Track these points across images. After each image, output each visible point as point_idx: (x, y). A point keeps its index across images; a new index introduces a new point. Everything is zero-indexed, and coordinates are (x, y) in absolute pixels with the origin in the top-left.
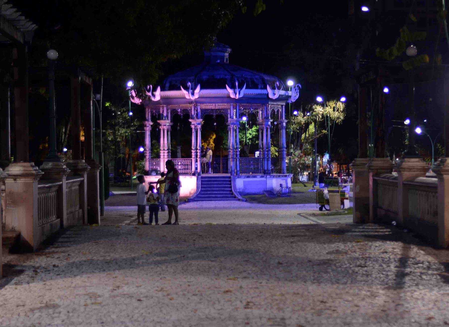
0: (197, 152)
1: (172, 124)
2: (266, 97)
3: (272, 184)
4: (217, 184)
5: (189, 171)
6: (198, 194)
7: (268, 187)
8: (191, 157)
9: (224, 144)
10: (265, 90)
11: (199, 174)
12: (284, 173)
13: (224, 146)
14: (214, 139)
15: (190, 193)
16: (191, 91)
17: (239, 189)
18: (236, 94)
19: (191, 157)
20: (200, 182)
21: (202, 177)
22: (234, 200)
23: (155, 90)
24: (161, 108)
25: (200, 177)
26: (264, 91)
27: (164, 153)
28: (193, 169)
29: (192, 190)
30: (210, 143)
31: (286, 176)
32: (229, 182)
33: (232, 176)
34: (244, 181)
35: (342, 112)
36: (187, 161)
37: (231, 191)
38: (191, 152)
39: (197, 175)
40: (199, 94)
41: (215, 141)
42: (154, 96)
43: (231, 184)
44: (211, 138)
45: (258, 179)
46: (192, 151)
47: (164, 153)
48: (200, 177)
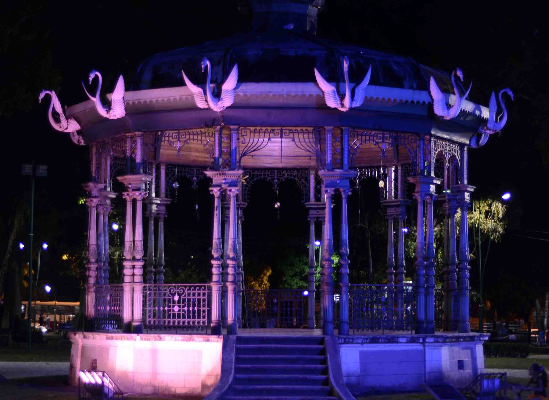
0: (224, 267)
1: (168, 201)
2: (425, 112)
3: (440, 361)
5: (202, 320)
6: (226, 393)
7: (428, 370)
8: (209, 277)
9: (285, 282)
10: (424, 93)
11: (231, 330)
12: (466, 331)
13: (284, 286)
14: (270, 276)
15: (204, 386)
16: (210, 86)
17: (348, 376)
18: (342, 97)
21: (240, 340)
23: (110, 88)
24: (128, 146)
25: (233, 337)
26: (420, 96)
27: (134, 267)
29: (209, 375)
30: (262, 281)
31: (472, 338)
32: (320, 354)
33: (327, 338)
34: (362, 353)
35: (500, 220)
37: (326, 382)
38: (211, 266)
39: (224, 332)
40: (236, 96)
41: (270, 278)
42: (107, 104)
43: (324, 361)
44: (265, 274)
45: (402, 347)
46: (214, 262)
47: (134, 267)
48: (233, 337)
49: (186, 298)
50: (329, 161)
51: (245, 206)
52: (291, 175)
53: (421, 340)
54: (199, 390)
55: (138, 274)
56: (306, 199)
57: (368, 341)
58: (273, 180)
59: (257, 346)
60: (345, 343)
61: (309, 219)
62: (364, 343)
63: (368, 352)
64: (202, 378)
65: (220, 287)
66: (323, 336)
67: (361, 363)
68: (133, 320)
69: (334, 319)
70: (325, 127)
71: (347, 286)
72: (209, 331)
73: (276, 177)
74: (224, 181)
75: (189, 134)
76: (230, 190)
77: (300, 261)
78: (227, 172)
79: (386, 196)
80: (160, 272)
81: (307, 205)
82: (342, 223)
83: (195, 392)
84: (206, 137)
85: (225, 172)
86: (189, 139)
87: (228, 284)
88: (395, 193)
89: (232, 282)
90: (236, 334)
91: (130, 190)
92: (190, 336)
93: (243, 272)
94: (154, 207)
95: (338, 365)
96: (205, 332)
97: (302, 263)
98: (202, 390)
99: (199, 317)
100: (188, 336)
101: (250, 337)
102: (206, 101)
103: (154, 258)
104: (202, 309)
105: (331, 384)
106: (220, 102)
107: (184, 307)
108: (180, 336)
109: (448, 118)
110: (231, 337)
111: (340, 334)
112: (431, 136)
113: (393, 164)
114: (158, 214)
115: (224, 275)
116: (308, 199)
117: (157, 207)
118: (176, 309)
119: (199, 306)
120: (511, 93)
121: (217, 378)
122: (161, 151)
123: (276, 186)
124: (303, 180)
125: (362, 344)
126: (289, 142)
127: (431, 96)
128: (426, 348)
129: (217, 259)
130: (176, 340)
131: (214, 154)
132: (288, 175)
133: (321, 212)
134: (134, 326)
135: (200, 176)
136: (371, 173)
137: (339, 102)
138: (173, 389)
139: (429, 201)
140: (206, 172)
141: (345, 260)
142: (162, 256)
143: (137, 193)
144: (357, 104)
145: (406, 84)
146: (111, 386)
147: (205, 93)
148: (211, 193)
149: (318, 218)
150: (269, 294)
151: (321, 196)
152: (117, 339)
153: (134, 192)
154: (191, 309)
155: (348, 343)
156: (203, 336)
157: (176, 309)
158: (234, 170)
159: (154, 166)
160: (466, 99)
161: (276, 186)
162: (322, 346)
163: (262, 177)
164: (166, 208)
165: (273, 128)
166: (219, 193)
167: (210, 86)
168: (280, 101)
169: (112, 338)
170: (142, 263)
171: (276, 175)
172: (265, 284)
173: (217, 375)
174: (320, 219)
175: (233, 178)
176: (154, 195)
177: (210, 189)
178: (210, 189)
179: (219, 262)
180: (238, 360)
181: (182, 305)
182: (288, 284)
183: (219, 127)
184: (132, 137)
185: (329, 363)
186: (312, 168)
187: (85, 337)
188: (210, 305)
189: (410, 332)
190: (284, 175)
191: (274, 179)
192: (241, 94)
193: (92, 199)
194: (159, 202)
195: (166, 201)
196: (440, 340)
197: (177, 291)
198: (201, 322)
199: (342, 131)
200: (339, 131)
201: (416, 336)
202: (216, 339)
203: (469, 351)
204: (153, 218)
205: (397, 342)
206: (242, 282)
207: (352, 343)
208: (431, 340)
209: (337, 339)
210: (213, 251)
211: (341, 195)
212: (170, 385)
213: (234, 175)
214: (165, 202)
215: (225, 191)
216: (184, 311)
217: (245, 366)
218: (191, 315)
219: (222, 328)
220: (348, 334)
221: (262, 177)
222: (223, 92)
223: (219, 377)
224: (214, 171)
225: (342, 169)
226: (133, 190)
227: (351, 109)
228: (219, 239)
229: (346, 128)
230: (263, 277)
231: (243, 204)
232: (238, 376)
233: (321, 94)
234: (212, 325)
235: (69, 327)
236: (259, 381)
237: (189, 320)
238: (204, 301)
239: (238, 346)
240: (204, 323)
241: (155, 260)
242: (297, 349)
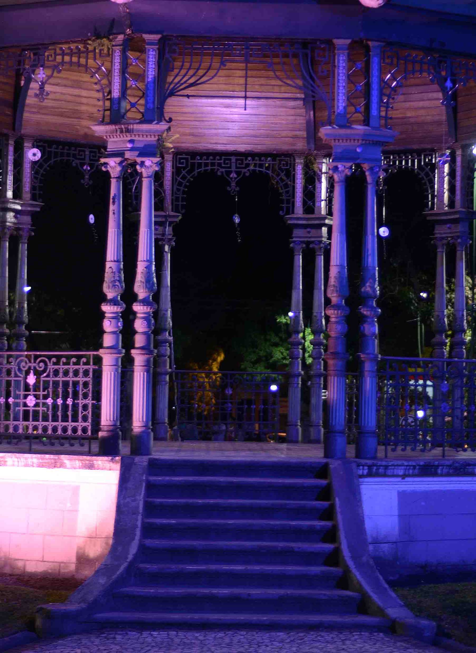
0: (128, 317)
1: (37, 206)
4: (244, 511)
5: (80, 424)
6: (122, 580)
11: (139, 446)
14: (222, 362)
15: (82, 559)
17: (376, 542)
19: (99, 346)
20: (141, 498)
21: (156, 466)
22: (359, 627)
25: (142, 461)
28: (108, 413)
32: (320, 497)
33: (334, 464)
34: (402, 495)
36: (69, 368)
37: (334, 558)
38: (102, 315)
39: (125, 448)
41: (222, 366)
43: (329, 514)
44: (215, 360)
46: (105, 308)
48: (142, 461)
49: (51, 379)
50: (341, 108)
51: (177, 220)
52: (261, 166)
54: (72, 567)
56: (288, 209)
57: (416, 471)
58: (229, 173)
59: (191, 478)
60: (370, 475)
61: (291, 245)
62: (409, 476)
63: (414, 493)
64: (80, 542)
65: (117, 359)
66: (325, 460)
67: (401, 516)
70: (335, 41)
72: (95, 447)
73: (233, 169)
74: (129, 145)
75: (63, 54)
76: (142, 164)
77: (266, 340)
78: (136, 127)
79: (433, 204)
80: (18, 337)
81: (291, 219)
82: (366, 234)
83: (62, 571)
84: (95, 59)
85: (131, 127)
86: (63, 63)
87: (133, 351)
88: (450, 198)
89: (141, 348)
90: (148, 454)
92: (56, 457)
93: (171, 338)
94: (10, 216)
95: (357, 521)
96: (86, 449)
97: (268, 343)
98: (77, 569)
99: (75, 419)
100: (52, 456)
101: (178, 461)
103: (7, 310)
104: (81, 402)
105: (345, 562)
107: (46, 397)
108: (34, 456)
110: (137, 459)
111: (359, 455)
113: (448, 145)
114: (18, 229)
115: (127, 333)
116: (291, 210)
117: (15, 217)
118: (31, 401)
119: (75, 396)
121: (107, 543)
122: (26, 115)
123: (233, 184)
124: (283, 175)
125: (404, 476)
126: (258, 107)
129: (114, 302)
130: (26, 465)
131: (110, 92)
133: (314, 232)
136: (407, 163)
138: (20, 564)
141: (372, 307)
142: (23, 307)
148: (104, 169)
149: (308, 243)
150: (219, 391)
151: (314, 205)
154: (70, 401)
155: (377, 475)
156: (81, 457)
157: (31, 401)
159: (11, 142)
161: (233, 184)
162: (324, 482)
163: (209, 168)
164: (32, 220)
166: (119, 169)
171: (233, 165)
173: (107, 538)
174: (311, 246)
175: (149, 139)
176: (10, 194)
177: (103, 160)
178: (103, 160)
180: (150, 509)
182: (248, 374)
183: (121, 37)
185: (339, 517)
186: (301, 153)
188: (97, 396)
190: (248, 165)
191: (231, 172)
194: (19, 207)
195: (32, 205)
197: (33, 365)
198: (40, 427)
202: (108, 465)
204: (8, 236)
206: (170, 357)
207: (385, 475)
209: (354, 466)
210: (105, 285)
211: (365, 176)
212: (14, 555)
213: (149, 133)
214: (29, 209)
215: (134, 164)
217: (165, 521)
218: (59, 414)
219: (120, 442)
220: (375, 458)
221: (209, 168)
223: (111, 542)
225: (368, 125)
228: (118, 261)
229: (376, 44)
230: (212, 365)
231: (174, 216)
232: (148, 542)
236: (192, 555)
239: (152, 478)
240: (84, 430)
241: (11, 314)
242: (271, 486)
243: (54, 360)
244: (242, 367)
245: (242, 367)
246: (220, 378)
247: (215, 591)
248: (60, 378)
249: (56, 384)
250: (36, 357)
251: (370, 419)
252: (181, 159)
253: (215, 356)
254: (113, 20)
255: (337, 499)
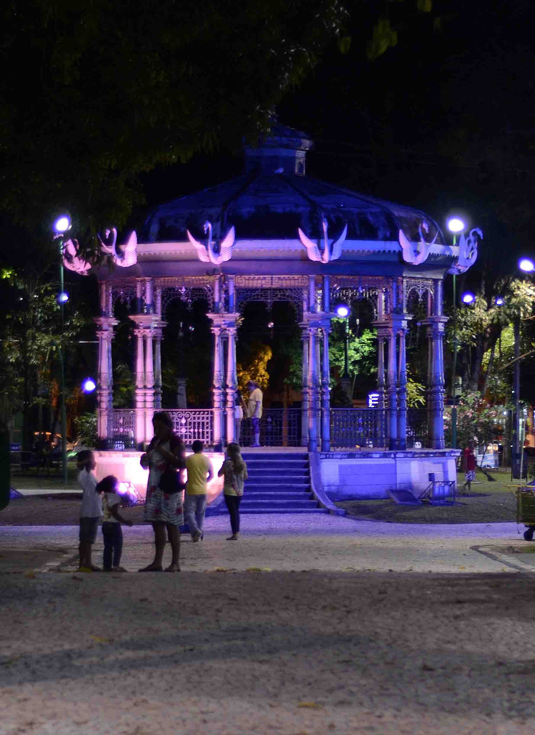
0: (225, 394)
1: (165, 324)
3: (410, 473)
7: (398, 481)
8: (210, 405)
9: (293, 373)
10: (394, 243)
12: (439, 448)
13: (291, 380)
16: (211, 243)
18: (322, 251)
19: (212, 406)
23: (123, 239)
26: (391, 246)
28: (217, 435)
30: (257, 370)
32: (304, 467)
33: (311, 454)
34: (340, 467)
36: (201, 416)
37: (309, 489)
38: (212, 394)
39: (224, 449)
40: (233, 252)
42: (121, 254)
43: (308, 473)
44: (261, 359)
45: (376, 461)
46: (215, 391)
49: (193, 421)
53: (393, 456)
55: (150, 400)
60: (326, 458)
68: (145, 441)
69: (331, 439)
71: (328, 410)
74: (223, 323)
76: (229, 330)
87: (227, 409)
91: (142, 328)
95: (318, 476)
102: (208, 256)
104: (205, 430)
106: (219, 258)
107: (190, 429)
109: (417, 264)
110: (383, 388)
111: (322, 451)
112: (403, 277)
120: (480, 233)
123: (269, 306)
127: (401, 246)
128: (397, 462)
129: (218, 388)
132: (281, 295)
134: (147, 445)
135: (195, 298)
137: (320, 257)
139: (401, 334)
140: (207, 315)
143: (148, 331)
144: (335, 257)
145: (380, 234)
146: (135, 494)
147: (207, 249)
152: (133, 456)
153: (145, 330)
154: (201, 430)
155: (329, 458)
158: (231, 312)
160: (436, 242)
165: (265, 276)
167: (211, 243)
168: (271, 255)
169: (128, 456)
170: (153, 392)
171: (269, 296)
172: (261, 376)
179: (220, 391)
181: (188, 427)
184: (141, 281)
187: (101, 455)
188: (212, 427)
189: (384, 449)
190: (277, 295)
192: (237, 250)
193: (103, 332)
196: (409, 455)
199: (323, 278)
200: (321, 278)
201: (387, 452)
203: (441, 465)
205: (371, 457)
207: (332, 458)
208: (402, 455)
209: (319, 454)
216: (190, 432)
220: (329, 451)
222: (222, 248)
224: (215, 314)
226: (144, 328)
227: (330, 261)
228: (220, 371)
233: (304, 249)
234: (214, 444)
235: (17, 448)
237: (190, 440)
238: (207, 423)
242: (286, 463)
243: (193, 413)
244: (291, 370)
245: (291, 370)
246: (268, 380)
247: (263, 501)
248: (196, 421)
249: (194, 423)
250: (185, 412)
251: (327, 435)
252: (240, 292)
253: (262, 355)
254: (215, 269)
255: (311, 468)
